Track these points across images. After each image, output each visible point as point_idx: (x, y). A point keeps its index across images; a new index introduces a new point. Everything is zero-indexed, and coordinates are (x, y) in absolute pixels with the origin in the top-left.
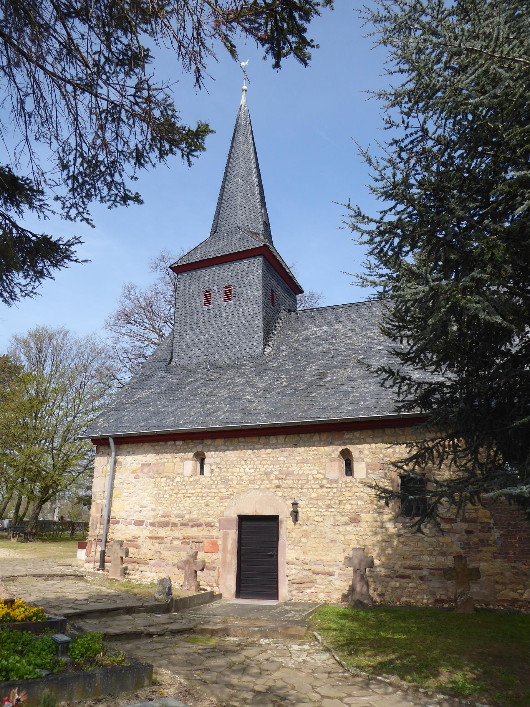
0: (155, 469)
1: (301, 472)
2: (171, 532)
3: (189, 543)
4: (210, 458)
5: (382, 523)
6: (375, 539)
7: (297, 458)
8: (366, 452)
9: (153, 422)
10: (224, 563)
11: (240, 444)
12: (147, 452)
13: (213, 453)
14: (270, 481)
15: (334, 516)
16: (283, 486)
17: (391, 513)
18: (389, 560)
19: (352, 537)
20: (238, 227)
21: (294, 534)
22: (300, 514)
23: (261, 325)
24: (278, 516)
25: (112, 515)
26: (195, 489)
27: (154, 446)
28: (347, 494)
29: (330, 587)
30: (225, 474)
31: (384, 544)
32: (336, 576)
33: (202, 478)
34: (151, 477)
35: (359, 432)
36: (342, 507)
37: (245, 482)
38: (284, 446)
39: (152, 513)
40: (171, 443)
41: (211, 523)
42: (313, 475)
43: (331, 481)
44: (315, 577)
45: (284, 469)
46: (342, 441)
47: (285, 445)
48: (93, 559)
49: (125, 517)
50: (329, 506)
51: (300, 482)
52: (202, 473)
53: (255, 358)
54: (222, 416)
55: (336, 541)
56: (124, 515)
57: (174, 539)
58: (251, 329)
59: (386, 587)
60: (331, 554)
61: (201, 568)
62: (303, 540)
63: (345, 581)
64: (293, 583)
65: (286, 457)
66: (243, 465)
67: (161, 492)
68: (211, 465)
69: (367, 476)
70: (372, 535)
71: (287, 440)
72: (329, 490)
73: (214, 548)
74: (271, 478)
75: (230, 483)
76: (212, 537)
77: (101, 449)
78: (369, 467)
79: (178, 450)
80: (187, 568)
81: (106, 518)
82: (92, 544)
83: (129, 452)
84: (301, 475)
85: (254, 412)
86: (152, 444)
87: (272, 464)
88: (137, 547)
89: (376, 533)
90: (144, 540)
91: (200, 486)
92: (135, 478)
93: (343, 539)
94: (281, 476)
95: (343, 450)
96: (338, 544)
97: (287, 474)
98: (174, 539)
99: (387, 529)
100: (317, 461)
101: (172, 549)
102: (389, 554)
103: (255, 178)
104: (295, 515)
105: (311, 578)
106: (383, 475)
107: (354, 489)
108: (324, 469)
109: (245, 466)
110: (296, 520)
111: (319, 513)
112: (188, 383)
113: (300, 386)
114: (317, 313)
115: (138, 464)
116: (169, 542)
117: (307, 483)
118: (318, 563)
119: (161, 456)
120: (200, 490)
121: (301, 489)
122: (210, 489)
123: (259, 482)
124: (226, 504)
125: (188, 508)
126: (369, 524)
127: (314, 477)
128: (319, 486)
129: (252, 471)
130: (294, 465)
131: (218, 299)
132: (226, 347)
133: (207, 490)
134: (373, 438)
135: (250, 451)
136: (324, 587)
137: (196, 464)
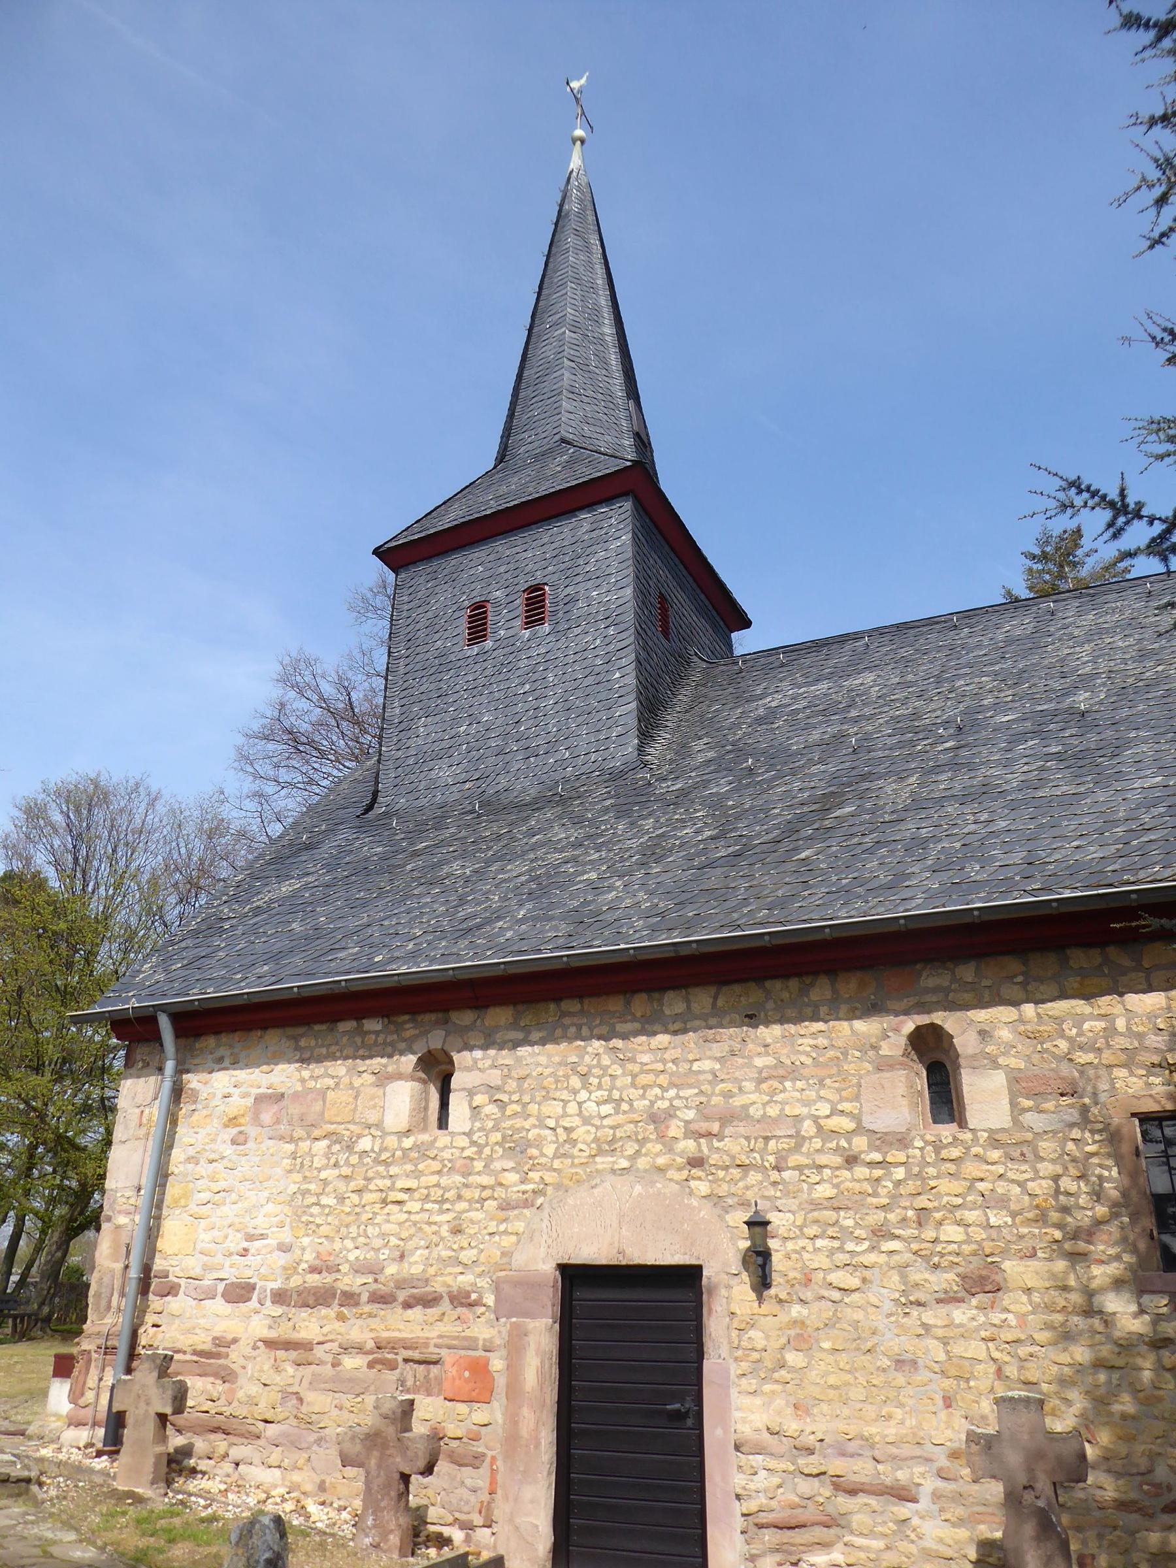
0: (295, 1110)
1: (773, 1111)
2: (337, 1325)
3: (392, 1366)
4: (468, 1069)
5: (1090, 1294)
6: (1065, 1358)
7: (759, 1062)
8: (1005, 1034)
9: (297, 961)
10: (512, 1440)
11: (567, 1021)
12: (275, 1058)
13: (478, 1054)
14: (669, 1144)
16: (714, 1159)
17: (1118, 1258)
18: (1129, 1439)
19: (976, 1349)
20: (563, 440)
21: (756, 1336)
22: (777, 1260)
23: (631, 680)
24: (699, 1268)
25: (159, 1264)
26: (418, 1174)
27: (295, 1038)
28: (945, 1185)
29: (904, 1545)
30: (518, 1123)
31: (1102, 1377)
32: (924, 1504)
33: (443, 1139)
34: (282, 1138)
35: (972, 965)
36: (930, 1234)
37: (581, 1152)
38: (713, 1021)
39: (281, 1259)
40: (349, 1025)
42: (816, 1119)
43: (882, 1140)
44: (843, 1502)
45: (715, 1100)
46: (912, 1000)
47: (716, 1018)
48: (89, 1412)
49: (197, 1272)
50: (881, 1233)
51: (772, 1143)
52: (443, 1123)
53: (615, 776)
54: (509, 934)
55: (914, 1363)
56: (194, 1265)
57: (345, 1349)
58: (602, 696)
59: (1126, 1552)
60: (898, 1413)
61: (421, 1464)
62: (792, 1358)
63: (960, 1522)
64: (760, 1526)
66: (575, 1092)
67: (312, 1187)
68: (471, 1093)
69: (1015, 1121)
71: (720, 1002)
72: (878, 1173)
73: (477, 1384)
74: (672, 1133)
75: (534, 1152)
76: (470, 1344)
77: (141, 1051)
78: (1018, 1084)
79: (370, 1047)
80: (373, 1462)
81: (134, 1273)
82: (89, 1361)
83: (220, 1060)
84: (775, 1121)
85: (609, 917)
86: (290, 1031)
87: (672, 1085)
88: (227, 1376)
89: (1066, 1336)
90: (248, 1351)
91: (436, 1165)
92: (234, 1142)
93: (942, 1357)
94: (703, 1126)
95: (918, 1028)
96: (923, 1375)
97: (727, 1119)
98: (345, 1349)
99: (1108, 1320)
100: (825, 1073)
101: (339, 1384)
102: (1124, 1417)
103: (608, 330)
104: (759, 1263)
105: (830, 1509)
106: (1075, 1115)
107: (972, 1169)
108: (857, 1098)
109: (583, 1095)
110: (762, 1283)
112: (416, 854)
113: (759, 835)
114: (794, 656)
115: (245, 1095)
116: (329, 1358)
117: (797, 1148)
118: (852, 1447)
119: (317, 1069)
120: (434, 1179)
121: (778, 1168)
122: (466, 1174)
124: (520, 1226)
125: (394, 1241)
126: (1036, 1297)
127: (820, 1128)
128: (838, 1160)
129: (606, 1109)
130: (749, 1085)
131: (506, 623)
132: (530, 753)
133: (458, 1179)
134: (1025, 985)
135: (597, 1044)
136: (879, 1544)
137: (426, 1092)
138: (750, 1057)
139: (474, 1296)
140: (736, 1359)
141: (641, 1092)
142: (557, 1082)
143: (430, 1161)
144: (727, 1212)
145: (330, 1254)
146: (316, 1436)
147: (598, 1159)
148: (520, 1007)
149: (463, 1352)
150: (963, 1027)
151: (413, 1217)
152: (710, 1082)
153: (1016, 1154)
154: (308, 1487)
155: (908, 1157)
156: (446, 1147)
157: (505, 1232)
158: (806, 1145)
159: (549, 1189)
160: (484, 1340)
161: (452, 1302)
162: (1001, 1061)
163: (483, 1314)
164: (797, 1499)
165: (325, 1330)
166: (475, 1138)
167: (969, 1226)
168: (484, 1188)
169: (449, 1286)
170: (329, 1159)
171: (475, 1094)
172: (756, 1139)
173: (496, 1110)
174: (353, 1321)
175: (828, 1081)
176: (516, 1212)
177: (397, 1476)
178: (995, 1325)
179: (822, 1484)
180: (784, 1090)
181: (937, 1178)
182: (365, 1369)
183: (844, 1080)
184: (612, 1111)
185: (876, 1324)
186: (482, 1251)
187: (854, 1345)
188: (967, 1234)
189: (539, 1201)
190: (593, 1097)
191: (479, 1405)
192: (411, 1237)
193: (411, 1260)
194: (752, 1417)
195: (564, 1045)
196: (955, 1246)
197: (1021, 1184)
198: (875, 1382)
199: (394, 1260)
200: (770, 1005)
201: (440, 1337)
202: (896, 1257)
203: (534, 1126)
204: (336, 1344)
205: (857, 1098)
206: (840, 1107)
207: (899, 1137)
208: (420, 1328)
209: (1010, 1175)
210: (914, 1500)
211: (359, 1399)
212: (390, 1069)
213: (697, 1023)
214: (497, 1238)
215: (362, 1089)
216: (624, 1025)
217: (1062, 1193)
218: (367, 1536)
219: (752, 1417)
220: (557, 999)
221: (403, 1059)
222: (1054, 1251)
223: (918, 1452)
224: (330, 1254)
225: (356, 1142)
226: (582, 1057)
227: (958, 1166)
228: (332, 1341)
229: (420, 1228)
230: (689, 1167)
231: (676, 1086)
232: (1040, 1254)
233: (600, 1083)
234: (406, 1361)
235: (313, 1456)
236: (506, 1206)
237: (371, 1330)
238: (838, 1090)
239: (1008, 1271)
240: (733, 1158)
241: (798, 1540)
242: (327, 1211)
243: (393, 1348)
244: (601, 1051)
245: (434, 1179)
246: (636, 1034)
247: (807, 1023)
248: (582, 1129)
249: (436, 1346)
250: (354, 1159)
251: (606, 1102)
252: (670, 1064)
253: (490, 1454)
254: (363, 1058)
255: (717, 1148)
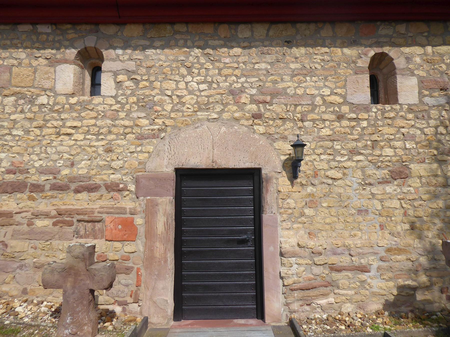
2: (29, 203)
3: (70, 224)
4: (114, 60)
6: (435, 205)
7: (293, 66)
8: (418, 60)
10: (150, 259)
11: (178, 36)
13: (120, 52)
14: (241, 106)
15: (363, 169)
16: (268, 114)
22: (303, 167)
24: (259, 170)
26: (81, 119)
28: (386, 130)
29: (363, 291)
30: (147, 92)
32: (373, 273)
36: (377, 152)
37: (188, 109)
38: (267, 43)
41: (118, 185)
42: (322, 96)
44: (335, 276)
45: (268, 84)
46: (375, 40)
47: (268, 41)
50: (354, 152)
51: (299, 108)
55: (367, 211)
57: (37, 216)
61: (106, 284)
62: (307, 211)
63: (390, 279)
64: (292, 290)
65: (271, 64)
66: (183, 76)
69: (421, 101)
70: (429, 200)
71: (271, 33)
73: (127, 231)
75: (159, 108)
76: (122, 211)
80: (69, 285)
84: (301, 96)
87: (243, 75)
89: (435, 196)
91: (93, 114)
93: (380, 208)
94: (261, 98)
95: (376, 54)
97: (275, 94)
98: (37, 216)
104: (293, 167)
108: (344, 87)
109: (189, 78)
111: (336, 164)
116: (25, 221)
117: (312, 111)
118: (339, 250)
120: (93, 122)
121: (302, 121)
122: (114, 119)
123: (219, 108)
125: (66, 156)
126: (424, 180)
127: (324, 101)
128: (333, 117)
130: (287, 78)
133: (109, 122)
134: (427, 37)
135: (197, 51)
138: (287, 63)
139: (121, 186)
140: (280, 213)
141: (224, 78)
142: (172, 70)
143: (89, 111)
144: (275, 142)
145: (21, 163)
146: (18, 264)
147: (199, 113)
148: (147, 26)
149: (117, 216)
150: (399, 55)
151: (78, 143)
152: (265, 75)
153: (420, 116)
154: (14, 293)
155: (369, 116)
156: (100, 104)
157: (141, 151)
158: (318, 109)
159: (169, 129)
160: (130, 208)
161: (107, 189)
162: (416, 72)
163: (128, 195)
164: (312, 276)
165: (20, 206)
166: (119, 99)
167: (396, 148)
168: (126, 127)
169: (105, 181)
170: (16, 108)
171: (118, 75)
172: (291, 105)
173: (132, 85)
174: (40, 200)
175: (330, 78)
176: (148, 141)
177: (88, 291)
178: (404, 193)
179: (325, 268)
180: (306, 81)
181: (381, 126)
182: (51, 226)
183: (338, 78)
184: (207, 88)
185: (350, 194)
186: (126, 161)
187: (338, 204)
188: (395, 152)
189: (163, 135)
190: (195, 80)
191: (128, 242)
192: (78, 154)
193: (79, 167)
194: (290, 240)
195: (176, 50)
196: (389, 158)
197: (421, 129)
198: (348, 220)
199: (67, 166)
200: (298, 37)
201: (101, 207)
202: (361, 163)
203: (158, 94)
204: (30, 213)
205: (344, 87)
206: (335, 91)
207: (365, 106)
208: (86, 203)
209: (417, 125)
210: (369, 272)
211: (48, 243)
212: (58, 56)
213: (258, 43)
214: (136, 155)
215: (39, 67)
216: (214, 42)
217: (438, 134)
218: (66, 329)
219: (290, 240)
220: (172, 23)
221: (68, 51)
222: (433, 159)
223: (371, 250)
224: (21, 163)
225: (36, 99)
226: (188, 58)
227: (393, 121)
228: (26, 211)
229: (84, 149)
230: (253, 119)
231: (245, 76)
232: (427, 161)
233: (199, 72)
234: (79, 221)
235: (17, 276)
236: (141, 137)
237: (53, 205)
238: (335, 83)
239: (413, 169)
240: (278, 114)
241: (311, 294)
242: (17, 138)
243: (70, 214)
244: (199, 55)
245: (93, 122)
246: (222, 46)
247: (319, 48)
248: (188, 97)
249: (99, 212)
250: (35, 109)
251: (203, 83)
252: (242, 64)
253: (136, 267)
254: (38, 49)
255: (269, 109)
